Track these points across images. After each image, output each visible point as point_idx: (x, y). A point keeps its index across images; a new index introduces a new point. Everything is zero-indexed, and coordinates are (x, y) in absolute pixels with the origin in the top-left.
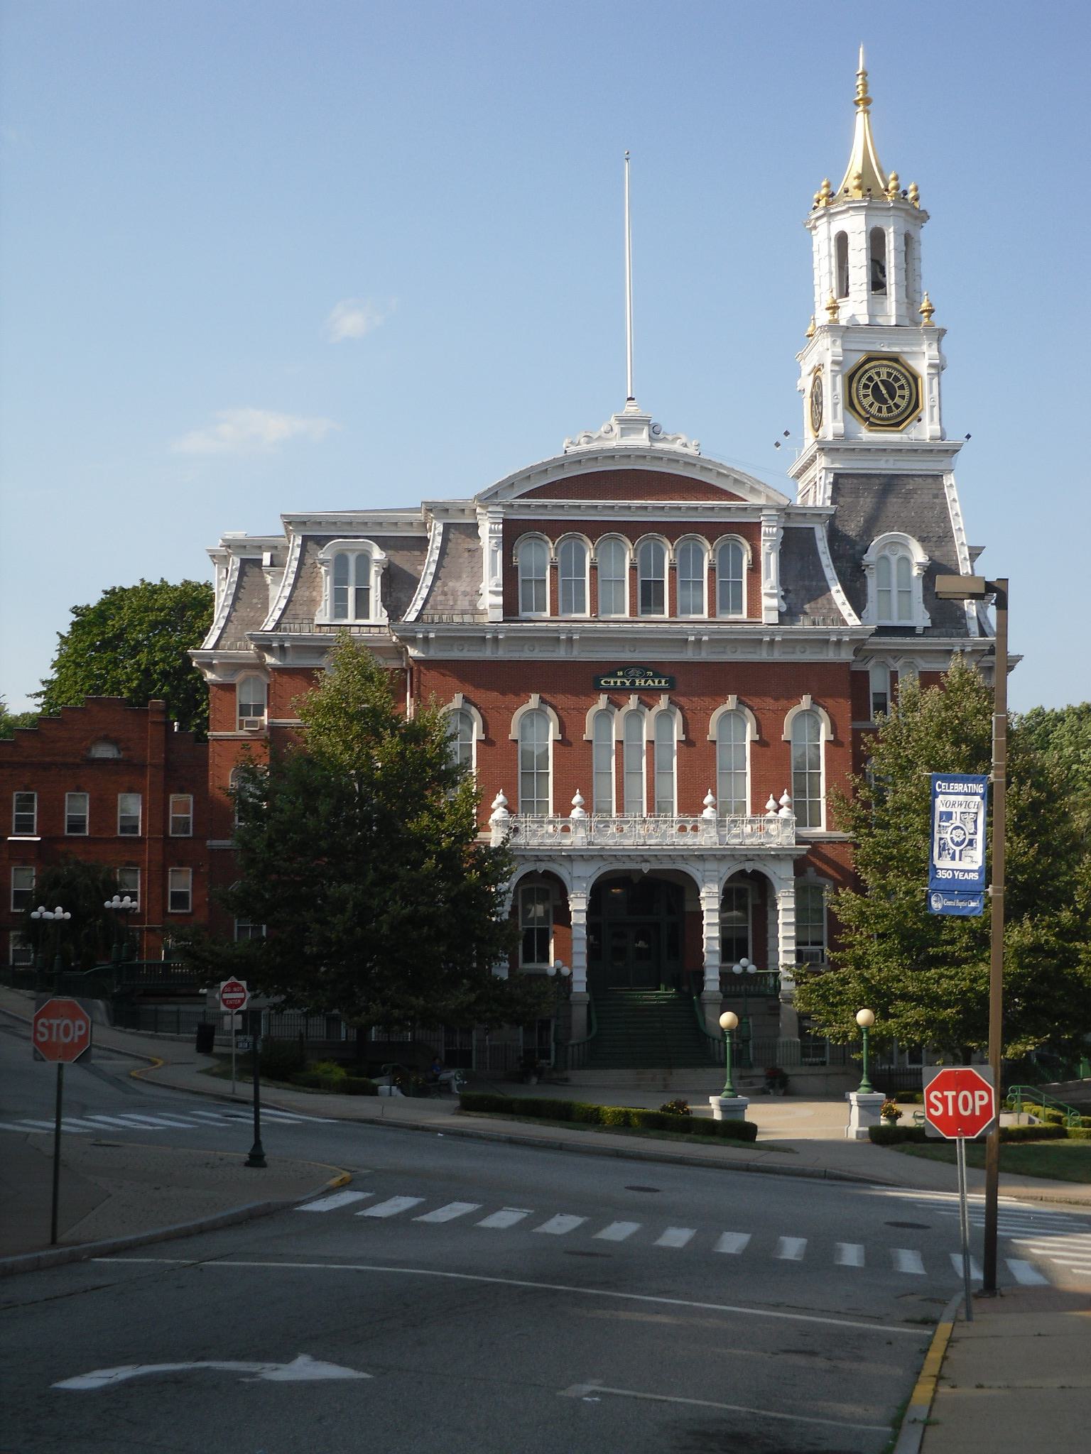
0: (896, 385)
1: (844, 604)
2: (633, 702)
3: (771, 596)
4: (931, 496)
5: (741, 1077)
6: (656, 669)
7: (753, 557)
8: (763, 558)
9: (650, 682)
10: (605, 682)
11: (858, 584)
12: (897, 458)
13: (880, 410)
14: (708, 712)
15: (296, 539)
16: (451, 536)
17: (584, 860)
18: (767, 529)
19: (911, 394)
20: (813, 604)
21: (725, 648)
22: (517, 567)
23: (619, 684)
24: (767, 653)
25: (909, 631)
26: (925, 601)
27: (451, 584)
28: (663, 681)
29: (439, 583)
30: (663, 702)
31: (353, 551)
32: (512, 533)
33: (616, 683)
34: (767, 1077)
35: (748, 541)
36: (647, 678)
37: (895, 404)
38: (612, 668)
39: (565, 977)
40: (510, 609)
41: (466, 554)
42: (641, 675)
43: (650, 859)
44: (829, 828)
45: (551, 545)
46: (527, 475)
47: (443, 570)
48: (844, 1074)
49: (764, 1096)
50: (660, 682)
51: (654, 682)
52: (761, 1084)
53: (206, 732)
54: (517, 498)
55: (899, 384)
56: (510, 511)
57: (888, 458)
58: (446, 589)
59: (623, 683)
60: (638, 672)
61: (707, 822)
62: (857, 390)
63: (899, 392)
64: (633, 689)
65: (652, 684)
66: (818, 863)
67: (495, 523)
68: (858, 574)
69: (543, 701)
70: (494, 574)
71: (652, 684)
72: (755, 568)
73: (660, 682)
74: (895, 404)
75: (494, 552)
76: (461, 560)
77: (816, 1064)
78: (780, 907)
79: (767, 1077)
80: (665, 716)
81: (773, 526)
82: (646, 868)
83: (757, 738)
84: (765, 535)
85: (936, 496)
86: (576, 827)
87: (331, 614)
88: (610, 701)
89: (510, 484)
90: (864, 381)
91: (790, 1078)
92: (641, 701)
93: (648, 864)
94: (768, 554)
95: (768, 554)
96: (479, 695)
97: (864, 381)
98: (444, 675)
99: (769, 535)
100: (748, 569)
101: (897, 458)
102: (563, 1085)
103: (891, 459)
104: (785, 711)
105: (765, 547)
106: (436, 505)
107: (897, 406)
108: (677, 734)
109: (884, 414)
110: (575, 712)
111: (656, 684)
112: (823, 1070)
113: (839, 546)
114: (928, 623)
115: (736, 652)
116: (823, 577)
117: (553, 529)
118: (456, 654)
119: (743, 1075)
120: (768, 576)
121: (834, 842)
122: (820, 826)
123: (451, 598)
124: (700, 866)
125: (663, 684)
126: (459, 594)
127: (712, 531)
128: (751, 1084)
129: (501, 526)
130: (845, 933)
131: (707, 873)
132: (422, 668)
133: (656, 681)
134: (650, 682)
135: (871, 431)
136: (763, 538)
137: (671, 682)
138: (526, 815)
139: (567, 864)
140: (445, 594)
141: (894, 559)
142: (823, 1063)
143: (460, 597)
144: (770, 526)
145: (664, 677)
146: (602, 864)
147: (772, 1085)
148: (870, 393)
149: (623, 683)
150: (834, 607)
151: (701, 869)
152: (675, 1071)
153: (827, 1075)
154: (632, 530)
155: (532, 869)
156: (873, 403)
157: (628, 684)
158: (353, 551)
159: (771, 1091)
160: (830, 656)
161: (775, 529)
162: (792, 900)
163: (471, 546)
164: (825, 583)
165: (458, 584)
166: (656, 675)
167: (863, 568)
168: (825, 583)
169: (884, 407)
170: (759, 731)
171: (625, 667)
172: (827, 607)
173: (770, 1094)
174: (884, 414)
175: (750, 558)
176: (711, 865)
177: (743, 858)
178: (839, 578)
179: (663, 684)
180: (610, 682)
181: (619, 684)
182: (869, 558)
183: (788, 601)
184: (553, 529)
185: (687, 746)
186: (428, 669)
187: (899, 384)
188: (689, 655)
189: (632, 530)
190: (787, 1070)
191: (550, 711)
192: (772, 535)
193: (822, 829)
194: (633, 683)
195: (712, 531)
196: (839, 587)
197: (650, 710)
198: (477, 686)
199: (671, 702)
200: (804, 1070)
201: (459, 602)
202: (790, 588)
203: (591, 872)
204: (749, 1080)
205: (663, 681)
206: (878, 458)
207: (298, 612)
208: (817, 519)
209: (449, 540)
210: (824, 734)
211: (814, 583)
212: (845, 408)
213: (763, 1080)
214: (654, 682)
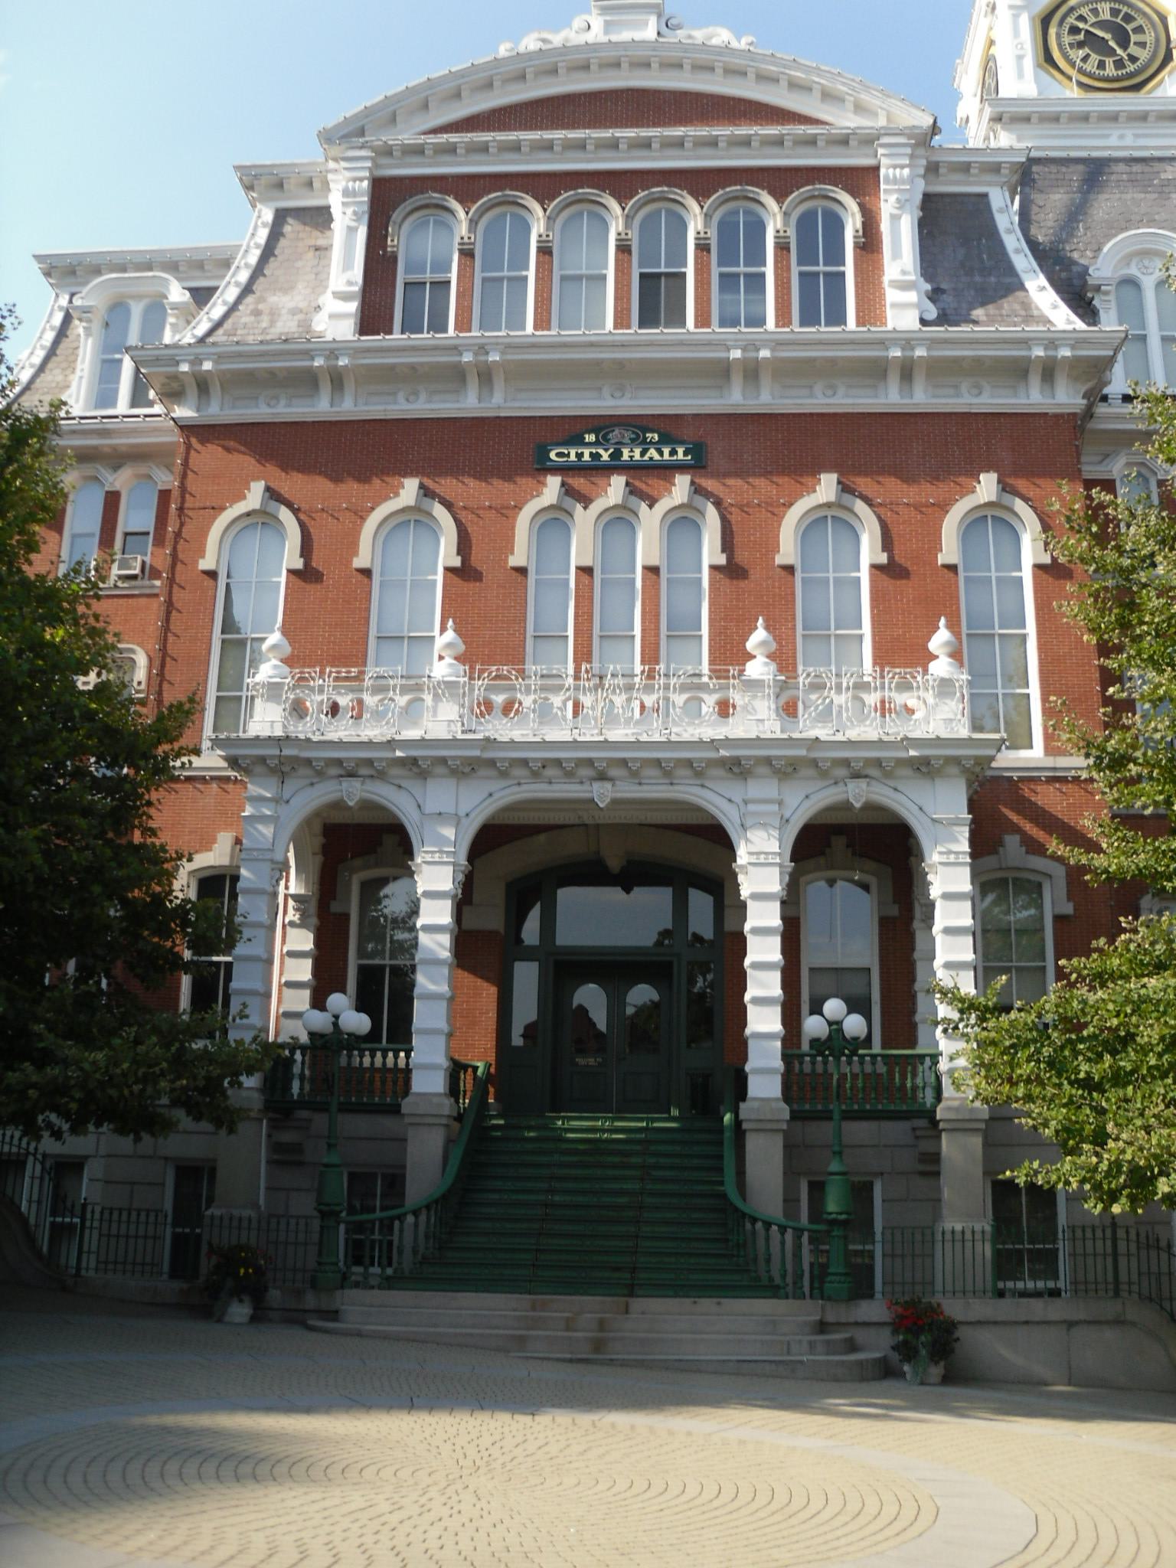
0: (1129, 27)
1: (1055, 307)
2: (616, 488)
3: (904, 286)
5: (822, 1327)
6: (668, 427)
7: (864, 224)
8: (885, 227)
9: (652, 453)
10: (558, 455)
12: (1140, 132)
13: (1101, 65)
14: (776, 510)
15: (60, 299)
16: (287, 229)
18: (891, 171)
19: (1157, 40)
20: (991, 308)
22: (394, 258)
23: (586, 457)
24: (901, 390)
28: (680, 451)
29: (250, 299)
30: (680, 488)
31: (139, 297)
33: (579, 456)
34: (897, 1326)
35: (854, 195)
37: (1129, 55)
38: (572, 430)
39: (333, 1033)
41: (311, 254)
42: (633, 440)
43: (614, 772)
44: (1049, 750)
45: (461, 213)
47: (261, 279)
48: (1119, 1322)
49: (886, 1384)
50: (673, 452)
51: (661, 453)
52: (879, 1344)
55: (1133, 25)
58: (261, 307)
59: (595, 456)
60: (628, 435)
61: (754, 685)
62: (1058, 36)
63: (1133, 38)
64: (616, 466)
65: (657, 457)
66: (1028, 827)
67: (355, 180)
69: (426, 492)
70: (347, 266)
71: (657, 457)
72: (870, 243)
73: (673, 452)
74: (1129, 55)
75: (351, 230)
77: (1037, 1294)
78: (935, 892)
79: (897, 1326)
80: (683, 522)
81: (902, 167)
83: (883, 558)
84: (887, 181)
86: (437, 697)
87: (87, 401)
88: (568, 490)
91: (962, 1332)
92: (632, 490)
93: (608, 785)
94: (895, 218)
95: (895, 218)
96: (293, 484)
98: (228, 450)
99: (895, 181)
100: (857, 246)
101: (1140, 132)
102: (326, 1331)
103: (1129, 133)
104: (944, 507)
105: (887, 205)
106: (259, 171)
107: (1133, 59)
108: (711, 552)
109: (1110, 70)
110: (493, 514)
111: (666, 456)
112: (1054, 1310)
115: (834, 394)
116: (1011, 270)
118: (261, 411)
119: (830, 1318)
120: (896, 255)
121: (1063, 780)
122: (1031, 747)
124: (736, 790)
125: (680, 455)
127: (781, 181)
128: (852, 1346)
129: (365, 184)
130: (1100, 951)
131: (751, 807)
132: (193, 441)
133: (666, 451)
134: (652, 453)
136: (883, 186)
138: (322, 673)
140: (257, 313)
141: (1148, 283)
142: (1055, 1293)
144: (895, 167)
145: (681, 443)
146: (495, 785)
147: (907, 1351)
149: (595, 456)
150: (1035, 313)
151: (737, 799)
152: (638, 1304)
153: (1071, 1324)
154: (621, 184)
155: (332, 797)
158: (139, 297)
159: (906, 1368)
160: (1033, 398)
161: (906, 171)
162: (966, 872)
163: (321, 242)
166: (666, 439)
167: (1089, 295)
168: (1015, 280)
169: (1109, 62)
170: (887, 543)
171: (603, 426)
172: (1023, 313)
173: (902, 1375)
174: (1110, 70)
175: (859, 225)
176: (762, 788)
177: (841, 772)
178: (1041, 266)
179: (680, 455)
180: (568, 455)
181: (586, 457)
185: (731, 578)
186: (202, 442)
187: (1133, 25)
188: (735, 399)
189: (621, 184)
190: (953, 1308)
191: (439, 511)
192: (903, 181)
193: (1035, 754)
194: (616, 455)
195: (781, 181)
196: (1042, 280)
197: (651, 506)
198: (285, 467)
199: (697, 490)
200: (1006, 1308)
201: (279, 324)
202: (944, 286)
204: (847, 1335)
205: (680, 451)
206: (1106, 132)
208: (989, 177)
209: (282, 235)
210: (1031, 551)
211: (993, 279)
212: (1038, 66)
213: (886, 1332)
214: (661, 453)
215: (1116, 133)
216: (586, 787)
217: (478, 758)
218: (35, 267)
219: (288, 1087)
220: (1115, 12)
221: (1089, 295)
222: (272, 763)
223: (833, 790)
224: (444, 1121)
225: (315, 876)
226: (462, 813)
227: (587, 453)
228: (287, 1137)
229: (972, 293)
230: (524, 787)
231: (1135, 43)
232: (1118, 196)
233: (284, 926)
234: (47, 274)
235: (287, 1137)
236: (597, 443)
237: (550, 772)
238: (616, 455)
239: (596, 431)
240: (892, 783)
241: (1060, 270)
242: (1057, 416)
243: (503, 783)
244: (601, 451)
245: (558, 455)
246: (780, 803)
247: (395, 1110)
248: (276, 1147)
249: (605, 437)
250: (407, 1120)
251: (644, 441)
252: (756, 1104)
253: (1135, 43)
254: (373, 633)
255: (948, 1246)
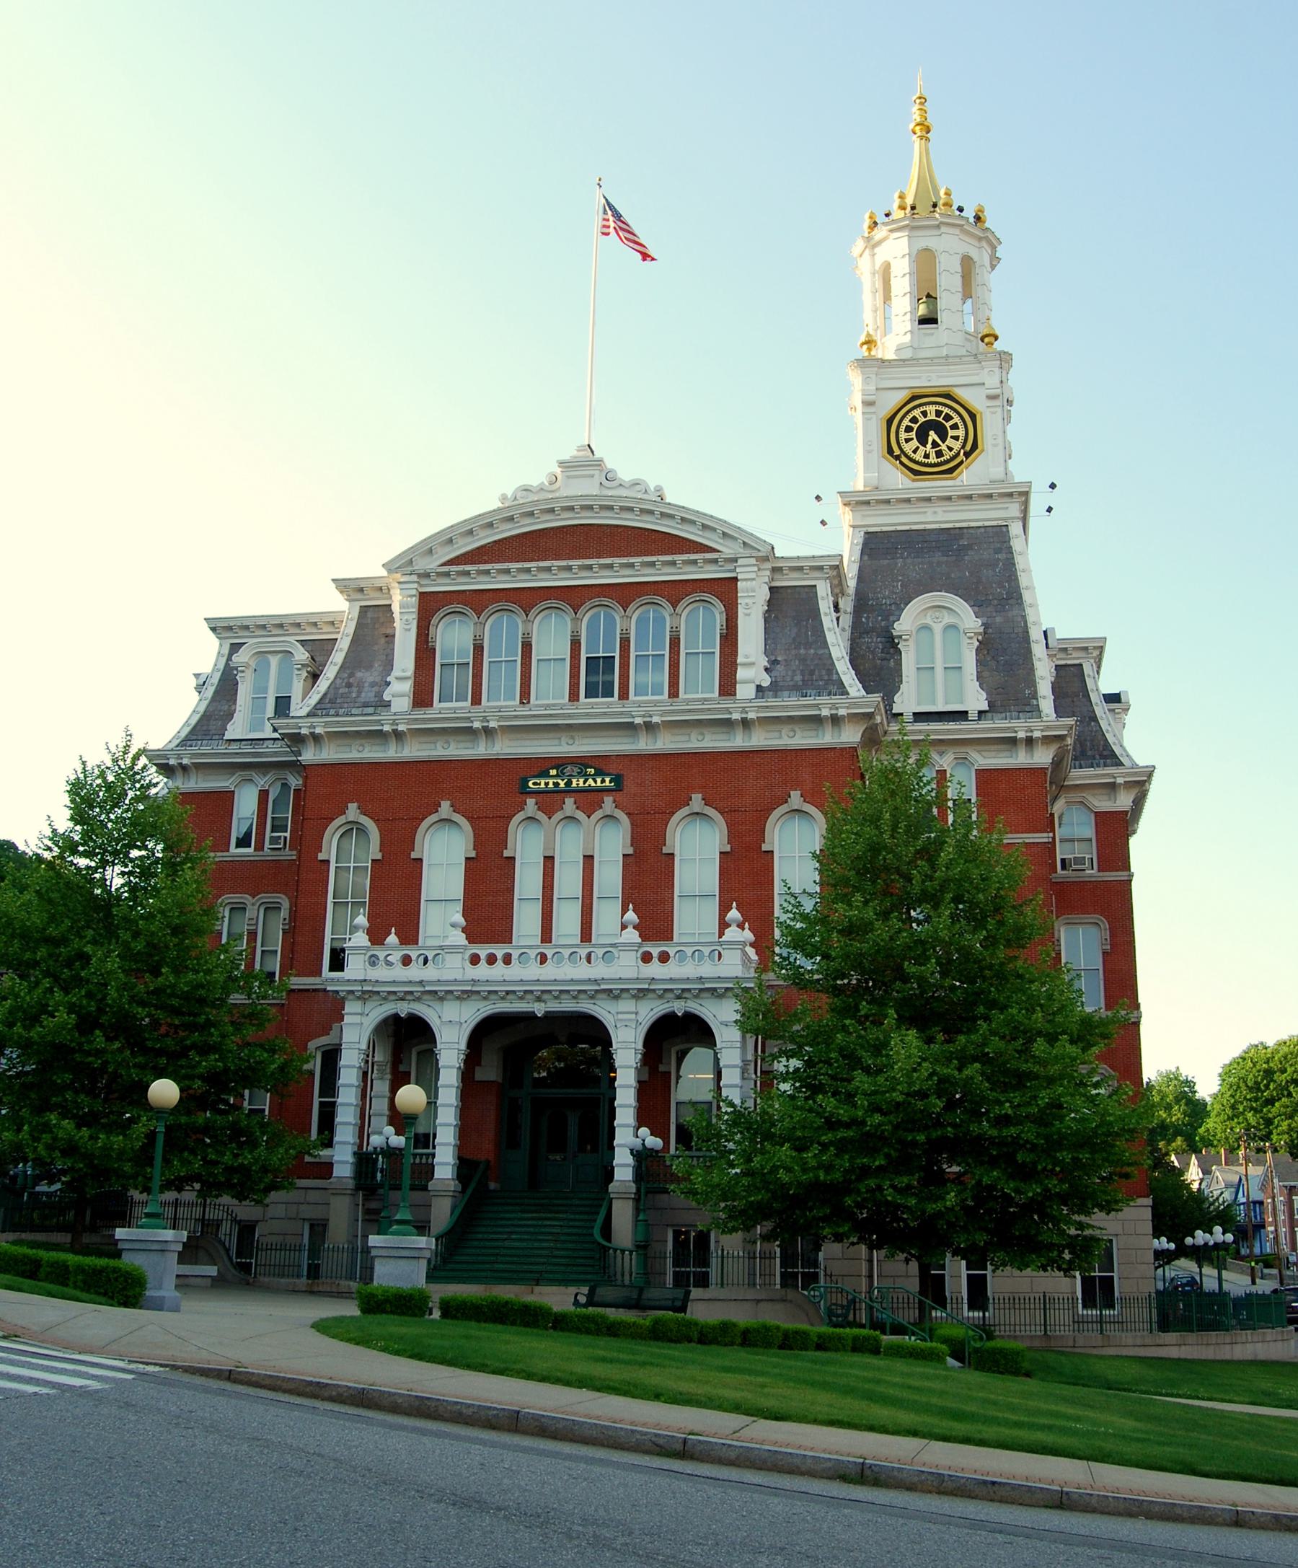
0: (948, 425)
4: (991, 551)
6: (600, 764)
9: (591, 782)
11: (892, 663)
17: (458, 998)
21: (689, 735)
23: (551, 785)
25: (962, 715)
26: (979, 677)
27: (359, 675)
28: (607, 780)
32: (429, 606)
33: (547, 784)
36: (586, 777)
38: (542, 766)
40: (422, 697)
46: (447, 538)
50: (603, 781)
51: (596, 782)
53: (922, 1174)
54: (442, 565)
55: (951, 423)
56: (424, 582)
57: (936, 509)
58: (351, 680)
59: (556, 784)
63: (951, 433)
65: (593, 784)
68: (892, 650)
71: (593, 784)
73: (603, 781)
76: (376, 648)
82: (539, 1009)
85: (998, 551)
89: (426, 547)
90: (906, 422)
93: (543, 1004)
97: (906, 422)
111: (599, 784)
113: (867, 618)
114: (985, 707)
117: (478, 602)
123: (355, 689)
125: (607, 783)
126: (366, 685)
127: (675, 592)
131: (620, 1016)
133: (599, 780)
134: (591, 782)
135: (914, 480)
137: (618, 780)
139: (436, 1005)
141: (938, 628)
143: (366, 689)
145: (608, 775)
148: (914, 437)
149: (556, 784)
153: (758, 1301)
155: (393, 1011)
156: (918, 448)
157: (562, 784)
164: (827, 651)
165: (368, 674)
166: (599, 772)
168: (827, 651)
171: (560, 763)
172: (826, 678)
176: (626, 1005)
179: (607, 783)
180: (540, 784)
181: (551, 785)
182: (901, 627)
183: (773, 674)
184: (478, 602)
187: (951, 423)
194: (569, 783)
195: (675, 592)
201: (363, 695)
203: (471, 1014)
205: (607, 780)
207: (211, 727)
208: (817, 574)
211: (812, 651)
214: (596, 782)
215: (930, 511)
216: (530, 1005)
217: (471, 991)
218: (205, 624)
219: (374, 1177)
220: (938, 413)
221: (896, 641)
222: (358, 994)
223: (667, 1005)
224: (451, 1194)
225: (389, 1052)
226: (463, 1021)
227: (551, 782)
228: (374, 1205)
229: (797, 662)
230: (497, 1005)
231: (952, 437)
232: (927, 560)
233: (372, 1081)
234: (213, 629)
235: (374, 1205)
236: (557, 776)
237: (510, 997)
238: (569, 783)
239: (556, 767)
240: (699, 1001)
241: (882, 620)
242: (841, 749)
243: (486, 1003)
244: (560, 781)
245: (534, 784)
246: (636, 1013)
247: (425, 1188)
248: (367, 1211)
249: (562, 772)
250: (431, 1193)
251: (586, 774)
252: (618, 1184)
253: (952, 437)
254: (423, 897)
255: (730, 1260)
